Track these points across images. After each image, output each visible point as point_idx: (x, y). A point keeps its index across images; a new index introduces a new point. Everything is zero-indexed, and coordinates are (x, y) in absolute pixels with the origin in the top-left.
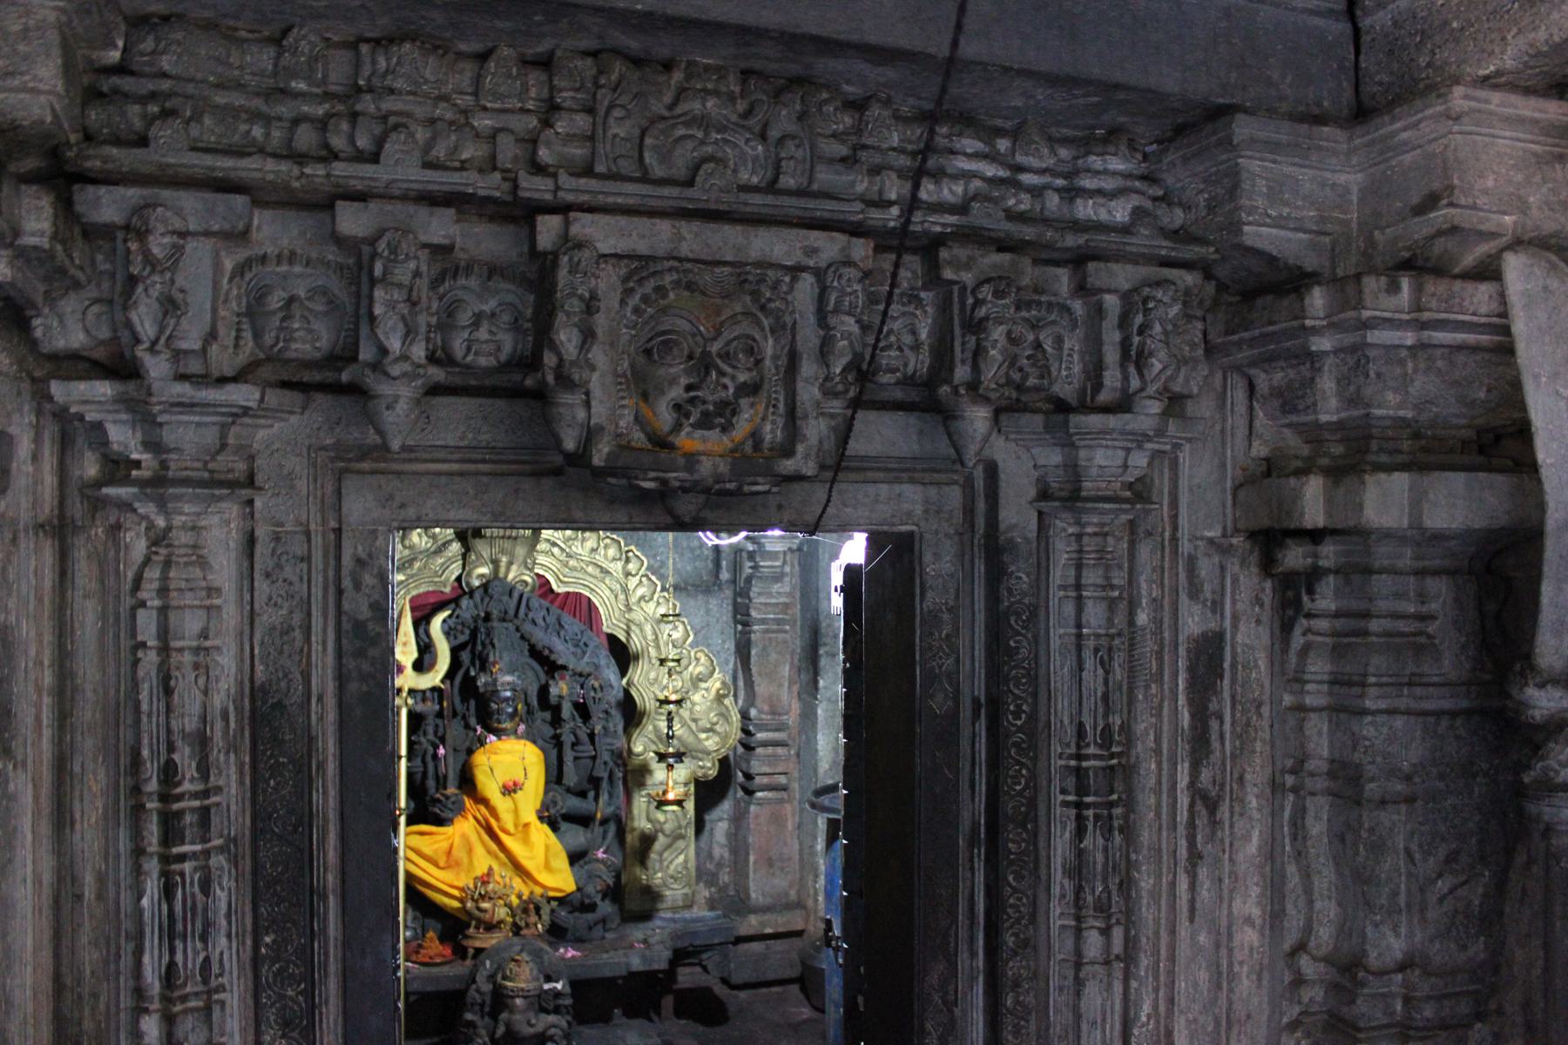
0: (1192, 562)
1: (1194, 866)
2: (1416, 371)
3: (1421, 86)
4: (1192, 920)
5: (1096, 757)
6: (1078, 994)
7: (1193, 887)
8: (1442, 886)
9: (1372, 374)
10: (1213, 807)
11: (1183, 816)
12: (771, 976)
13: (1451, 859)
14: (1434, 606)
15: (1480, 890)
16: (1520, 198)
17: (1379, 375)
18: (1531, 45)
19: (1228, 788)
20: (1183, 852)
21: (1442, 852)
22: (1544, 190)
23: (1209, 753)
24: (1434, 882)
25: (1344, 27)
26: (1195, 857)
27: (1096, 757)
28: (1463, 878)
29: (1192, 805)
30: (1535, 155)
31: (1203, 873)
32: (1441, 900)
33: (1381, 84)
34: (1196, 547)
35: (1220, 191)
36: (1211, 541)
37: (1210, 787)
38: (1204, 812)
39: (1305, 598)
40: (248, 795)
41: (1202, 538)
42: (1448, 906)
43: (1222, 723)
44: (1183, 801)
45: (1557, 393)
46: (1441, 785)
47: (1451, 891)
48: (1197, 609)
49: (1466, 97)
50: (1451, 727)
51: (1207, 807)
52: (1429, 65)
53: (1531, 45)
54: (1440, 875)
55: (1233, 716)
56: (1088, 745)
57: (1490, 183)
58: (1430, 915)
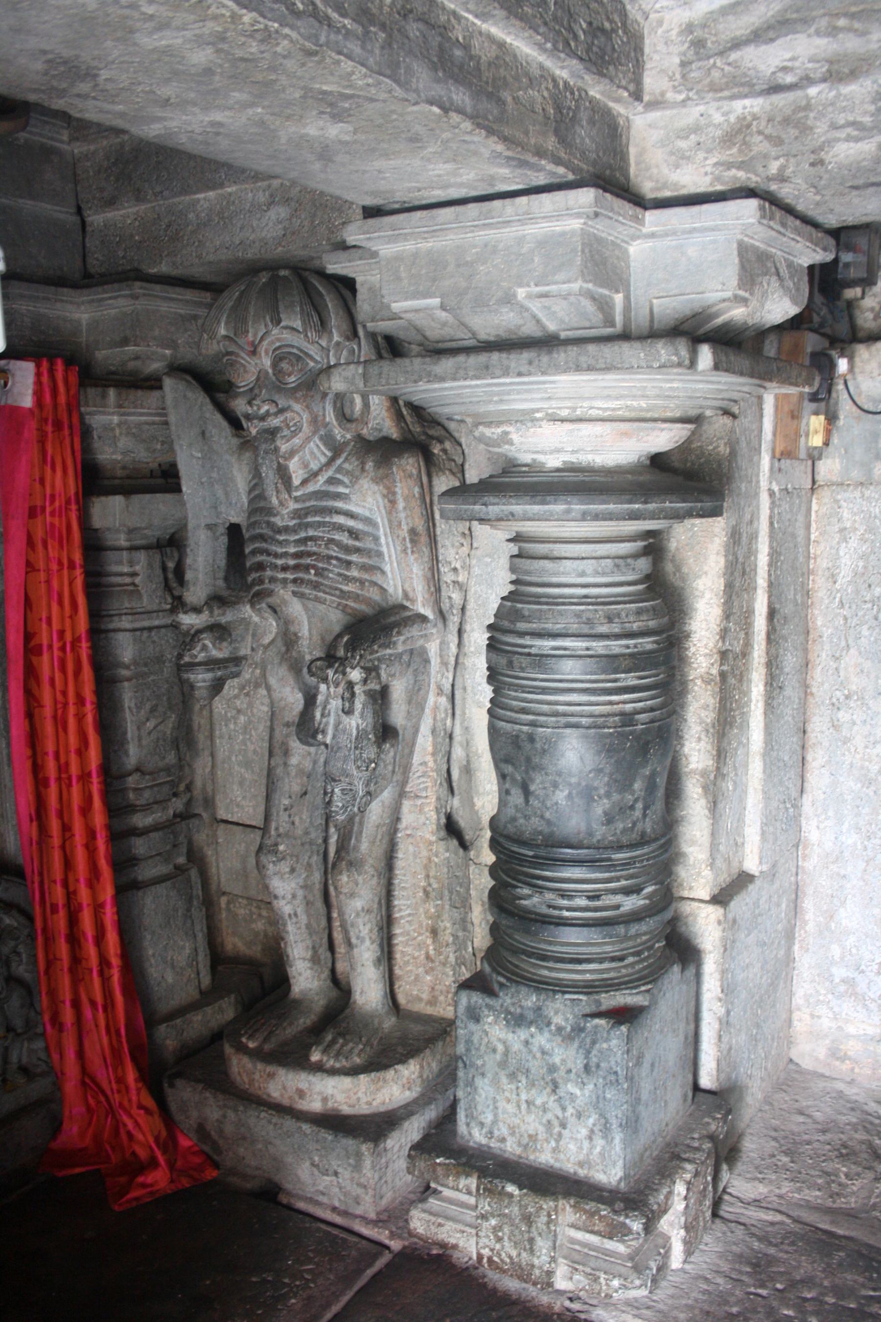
2: (121, 434)
8: (150, 725)
12: (324, 923)
13: (153, 710)
14: (137, 568)
15: (171, 725)
16: (173, 341)
17: (100, 437)
21: (148, 706)
22: (186, 336)
24: (144, 724)
25: (75, 219)
28: (160, 720)
30: (181, 315)
32: (149, 733)
33: (97, 260)
40: (47, 895)
42: (154, 736)
45: (192, 455)
46: (145, 669)
47: (155, 727)
49: (141, 288)
50: (149, 637)
52: (123, 257)
54: (148, 720)
57: (157, 333)
58: (144, 742)
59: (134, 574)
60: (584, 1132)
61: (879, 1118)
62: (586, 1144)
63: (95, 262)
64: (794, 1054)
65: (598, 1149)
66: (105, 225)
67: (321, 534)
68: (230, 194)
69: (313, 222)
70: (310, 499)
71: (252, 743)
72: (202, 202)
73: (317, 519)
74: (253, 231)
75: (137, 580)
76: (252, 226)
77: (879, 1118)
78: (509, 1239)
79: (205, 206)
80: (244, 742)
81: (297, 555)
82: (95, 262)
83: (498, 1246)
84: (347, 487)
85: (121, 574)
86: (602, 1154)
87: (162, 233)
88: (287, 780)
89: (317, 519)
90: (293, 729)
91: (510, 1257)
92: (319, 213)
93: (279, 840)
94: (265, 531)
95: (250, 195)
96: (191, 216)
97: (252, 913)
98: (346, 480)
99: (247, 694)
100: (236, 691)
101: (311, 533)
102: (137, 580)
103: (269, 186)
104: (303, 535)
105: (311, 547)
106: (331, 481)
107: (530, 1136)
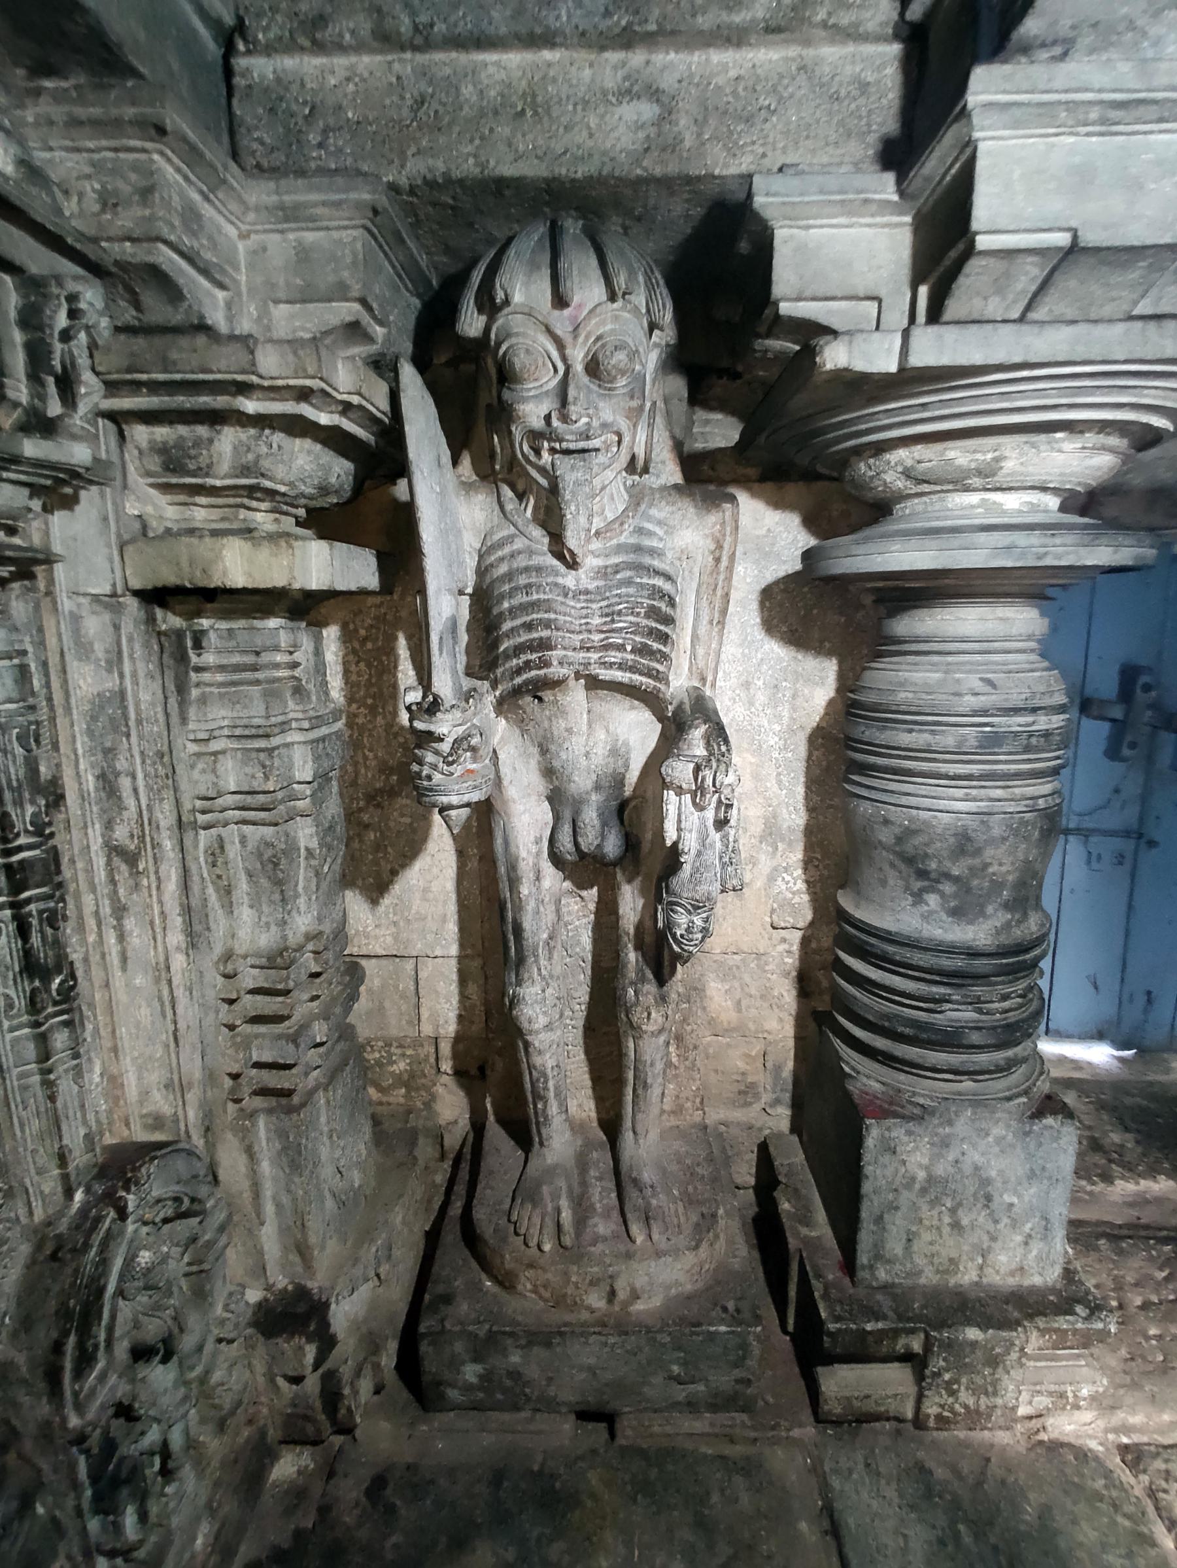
0: (76, 619)
1: (119, 919)
3: (313, 165)
4: (124, 968)
5: (30, 847)
6: (52, 1098)
7: (121, 937)
9: (275, 446)
10: (131, 859)
11: (101, 875)
14: (298, 656)
18: (430, 170)
19: (148, 839)
20: (106, 910)
23: (122, 808)
26: (120, 911)
27: (30, 847)
29: (109, 863)
31: (129, 923)
34: (79, 605)
35: (125, 189)
36: (96, 598)
37: (128, 842)
38: (124, 867)
39: (191, 653)
41: (85, 595)
43: (134, 777)
44: (100, 862)
48: (88, 669)
51: (126, 862)
53: (430, 170)
55: (144, 771)
56: (18, 835)
59: (295, 665)
60: (1019, 1238)
62: (1020, 1251)
63: (255, 146)
65: (1034, 1253)
66: (278, 80)
68: (549, 65)
69: (699, 135)
71: (388, 861)
72: (491, 70)
74: (591, 135)
76: (589, 128)
78: (967, 1389)
79: (497, 77)
80: (376, 862)
81: (613, 621)
82: (255, 146)
83: (951, 1400)
84: (661, 539)
85: (277, 666)
86: (1039, 1258)
87: (405, 112)
91: (966, 1407)
92: (712, 122)
95: (587, 72)
96: (467, 91)
98: (660, 532)
99: (378, 806)
100: (362, 803)
103: (624, 64)
107: (951, 1260)
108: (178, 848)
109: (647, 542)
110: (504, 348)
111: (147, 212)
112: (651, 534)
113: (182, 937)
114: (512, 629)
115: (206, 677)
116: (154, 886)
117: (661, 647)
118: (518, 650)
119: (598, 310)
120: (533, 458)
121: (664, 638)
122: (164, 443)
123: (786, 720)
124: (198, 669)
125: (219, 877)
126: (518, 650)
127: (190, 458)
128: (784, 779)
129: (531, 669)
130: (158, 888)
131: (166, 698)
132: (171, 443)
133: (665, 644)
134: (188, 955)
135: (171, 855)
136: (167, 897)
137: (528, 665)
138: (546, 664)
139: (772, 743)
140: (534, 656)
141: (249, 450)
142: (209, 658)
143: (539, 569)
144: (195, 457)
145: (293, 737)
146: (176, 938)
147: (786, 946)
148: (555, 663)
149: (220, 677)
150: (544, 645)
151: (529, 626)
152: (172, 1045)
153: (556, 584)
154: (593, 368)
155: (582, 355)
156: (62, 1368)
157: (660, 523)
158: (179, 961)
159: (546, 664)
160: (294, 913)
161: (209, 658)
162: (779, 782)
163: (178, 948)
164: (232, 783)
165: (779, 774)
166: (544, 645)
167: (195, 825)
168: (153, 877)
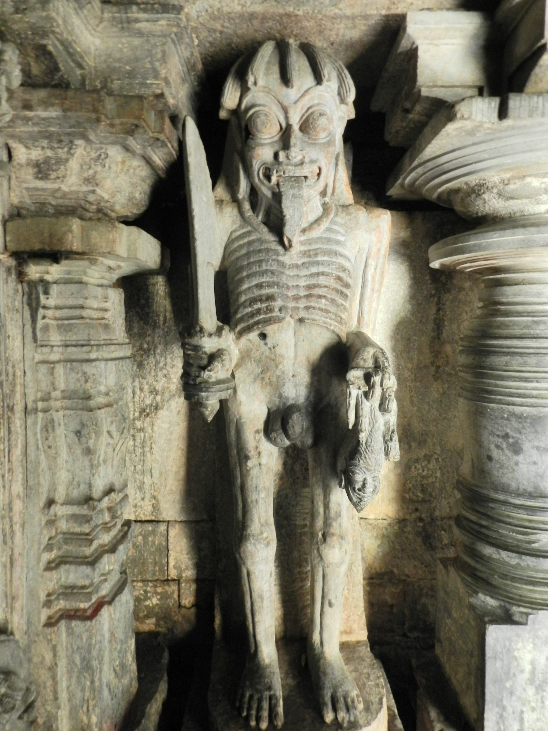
39: (42, 297)
61: (2, 642)
64: (495, 634)
67: (330, 271)
70: (316, 243)
73: (326, 258)
75: (107, 315)
77: (2, 642)
81: (309, 287)
84: (343, 235)
88: (261, 478)
89: (326, 258)
90: (262, 434)
93: (263, 528)
94: (275, 267)
97: (146, 592)
98: (341, 230)
101: (321, 269)
102: (107, 315)
104: (314, 270)
105: (322, 280)
106: (329, 230)
108: (23, 427)
109: (333, 236)
110: (250, 113)
111: (44, 14)
112: (337, 232)
113: (21, 489)
114: (249, 288)
115: (49, 313)
116: (7, 450)
117: (344, 303)
118: (254, 300)
119: (310, 91)
120: (266, 182)
121: (345, 296)
122: (37, 161)
123: (415, 361)
124: (44, 307)
125: (50, 447)
126: (254, 300)
127: (53, 171)
128: (415, 400)
129: (260, 314)
130: (9, 452)
131: (24, 325)
132: (41, 161)
133: (346, 300)
134: (23, 502)
135: (19, 430)
136: (14, 459)
137: (258, 311)
138: (271, 310)
139: (407, 376)
140: (264, 305)
141: (90, 168)
142: (51, 302)
143: (268, 250)
144: (55, 170)
145: (58, 404)
146: (18, 488)
147: (418, 514)
148: (277, 310)
149: (58, 314)
150: (270, 298)
151: (259, 286)
152: (8, 565)
153: (278, 261)
154: (305, 127)
155: (298, 119)
156: (466, 563)
157: (341, 225)
158: (18, 506)
159: (271, 310)
160: (96, 476)
161: (51, 302)
162: (412, 402)
163: (18, 496)
164: (61, 384)
165: (411, 397)
166: (270, 298)
167: (36, 410)
168: (6, 444)
